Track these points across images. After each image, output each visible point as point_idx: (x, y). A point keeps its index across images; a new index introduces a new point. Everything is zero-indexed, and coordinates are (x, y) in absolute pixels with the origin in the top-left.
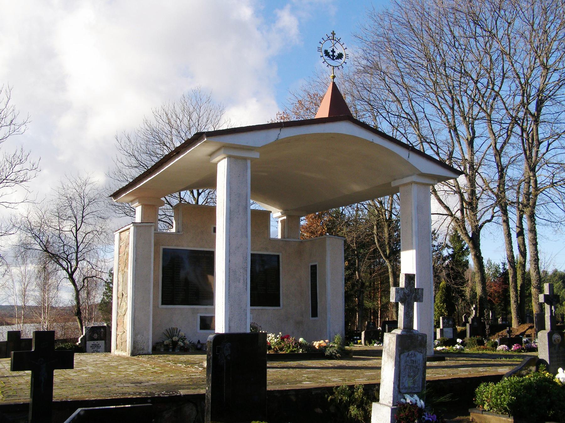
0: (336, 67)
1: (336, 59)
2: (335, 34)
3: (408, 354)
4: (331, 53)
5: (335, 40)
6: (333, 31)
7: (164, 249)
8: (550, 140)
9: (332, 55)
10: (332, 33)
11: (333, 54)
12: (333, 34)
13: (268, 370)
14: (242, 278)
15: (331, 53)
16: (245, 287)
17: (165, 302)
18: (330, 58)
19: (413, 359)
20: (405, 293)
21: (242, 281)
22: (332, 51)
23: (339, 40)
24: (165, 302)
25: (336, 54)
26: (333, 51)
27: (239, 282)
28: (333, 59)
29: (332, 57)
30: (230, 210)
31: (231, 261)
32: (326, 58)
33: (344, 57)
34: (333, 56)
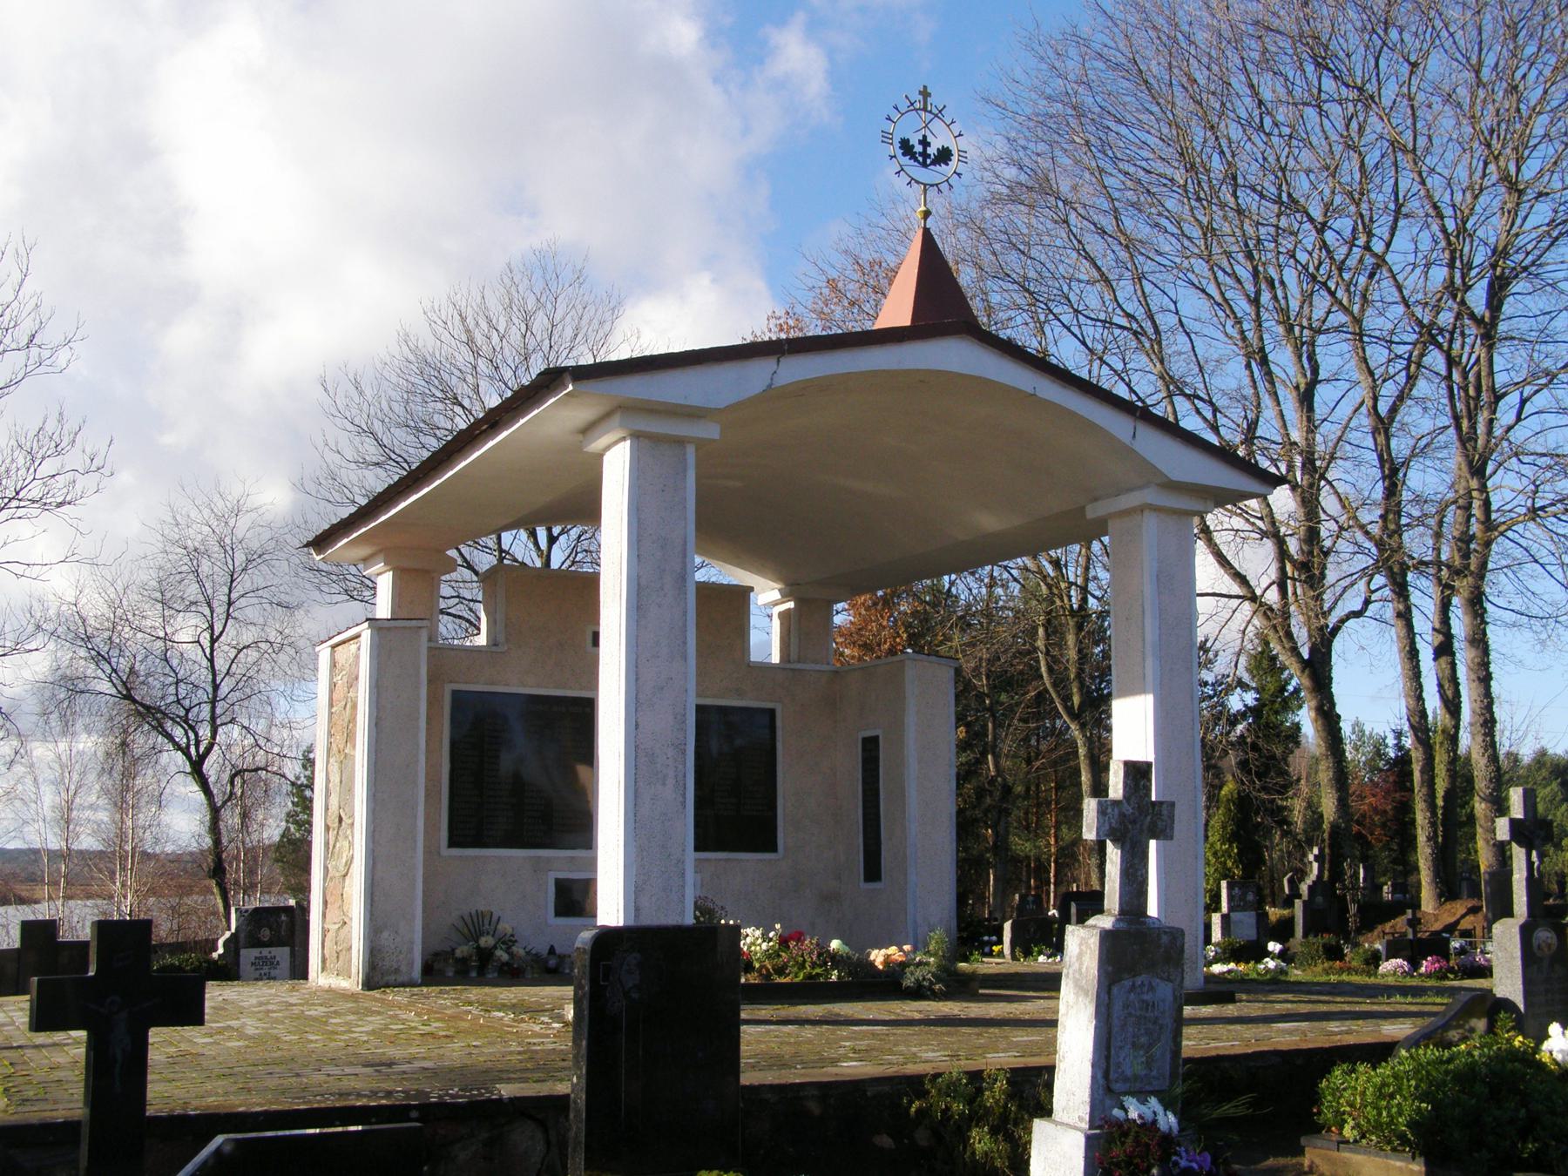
1: (933, 163)
2: (929, 95)
4: (918, 148)
11: (925, 149)
12: (925, 94)
13: (743, 1028)
15: (918, 148)
17: (457, 839)
18: (916, 160)
24: (457, 839)
25: (932, 151)
26: (925, 143)
28: (924, 165)
32: (906, 160)
34: (925, 155)
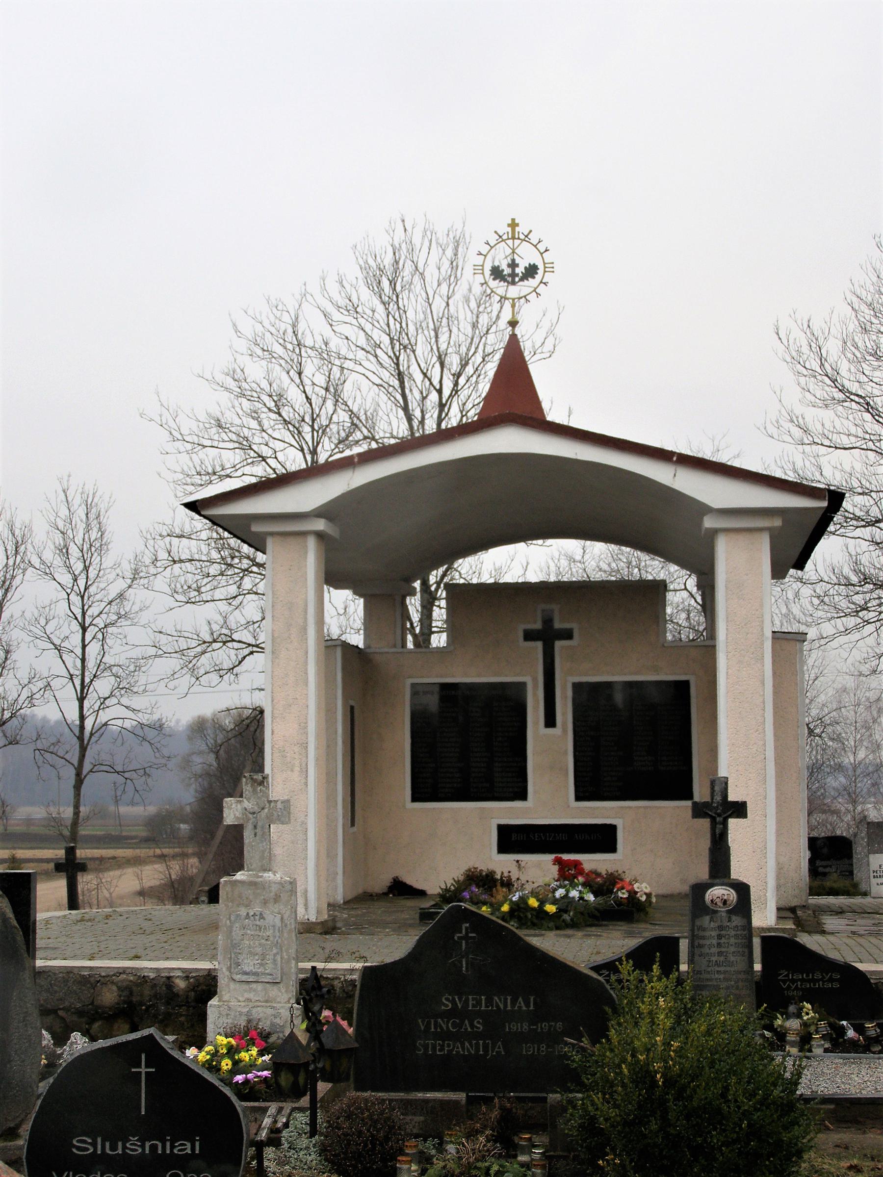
0: (520, 298)
1: (522, 280)
2: (517, 225)
3: (248, 914)
4: (507, 271)
5: (519, 238)
6: (513, 220)
7: (413, 685)
8: (255, 569)
9: (509, 275)
10: (509, 225)
11: (513, 271)
12: (513, 225)
14: (297, 763)
16: (304, 781)
19: (258, 923)
20: (246, 809)
21: (297, 769)
22: (509, 266)
23: (526, 236)
25: (520, 270)
26: (513, 265)
27: (292, 771)
29: (510, 279)
30: (273, 636)
31: (276, 732)
33: (540, 272)
